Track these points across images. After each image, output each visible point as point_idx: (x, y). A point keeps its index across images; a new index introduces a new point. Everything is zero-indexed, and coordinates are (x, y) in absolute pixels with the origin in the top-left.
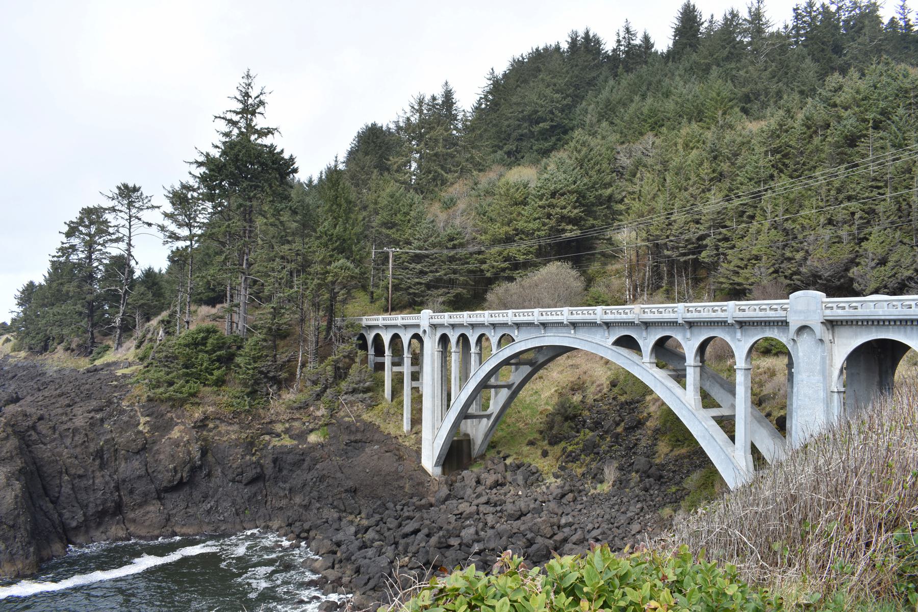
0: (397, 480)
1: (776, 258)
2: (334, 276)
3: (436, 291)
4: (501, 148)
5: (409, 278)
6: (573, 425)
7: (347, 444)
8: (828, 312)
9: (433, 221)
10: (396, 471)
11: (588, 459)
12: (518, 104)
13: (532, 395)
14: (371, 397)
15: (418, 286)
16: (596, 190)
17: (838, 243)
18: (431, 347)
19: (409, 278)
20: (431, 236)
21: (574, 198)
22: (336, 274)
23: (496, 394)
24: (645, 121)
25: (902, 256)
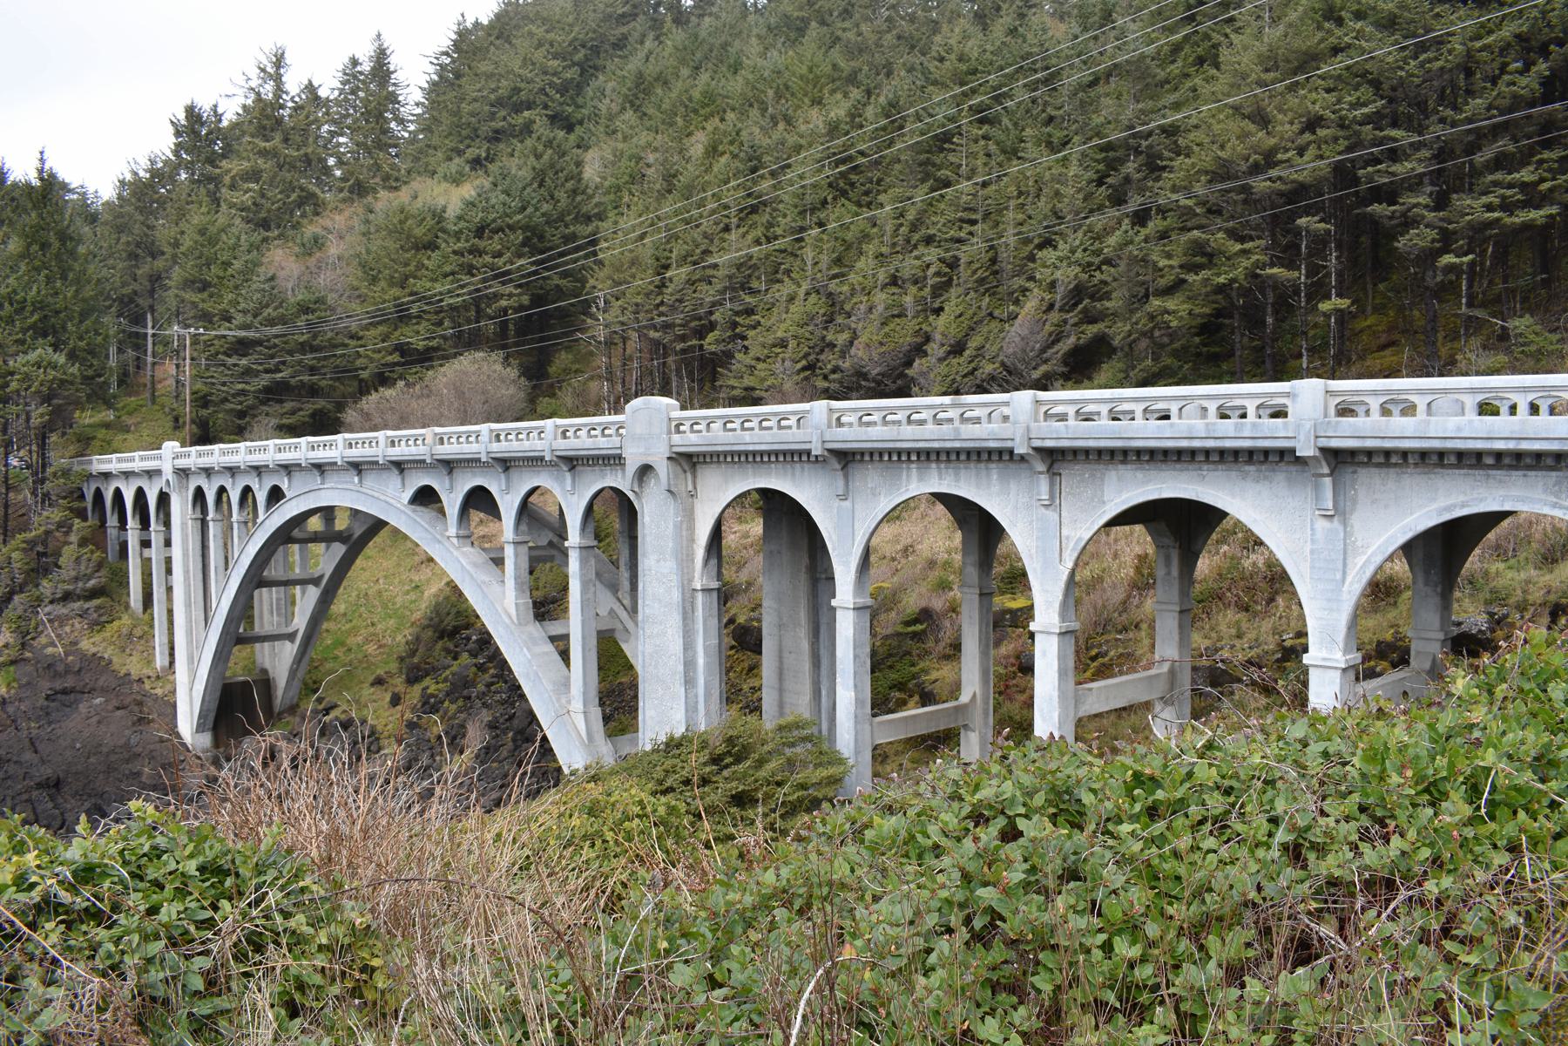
0: (128, 761)
1: (811, 343)
2: (23, 380)
3: (277, 407)
4: (460, 153)
5: (224, 384)
6: (451, 646)
7: (48, 698)
8: (676, 438)
9: (272, 278)
10: (127, 746)
11: (453, 707)
12: (489, 76)
13: (407, 593)
14: (98, 608)
15: (242, 399)
16: (566, 226)
17: (899, 316)
18: (180, 507)
19: (224, 384)
20: (267, 306)
21: (519, 237)
22: (27, 378)
23: (303, 593)
24: (695, 111)
25: (987, 339)
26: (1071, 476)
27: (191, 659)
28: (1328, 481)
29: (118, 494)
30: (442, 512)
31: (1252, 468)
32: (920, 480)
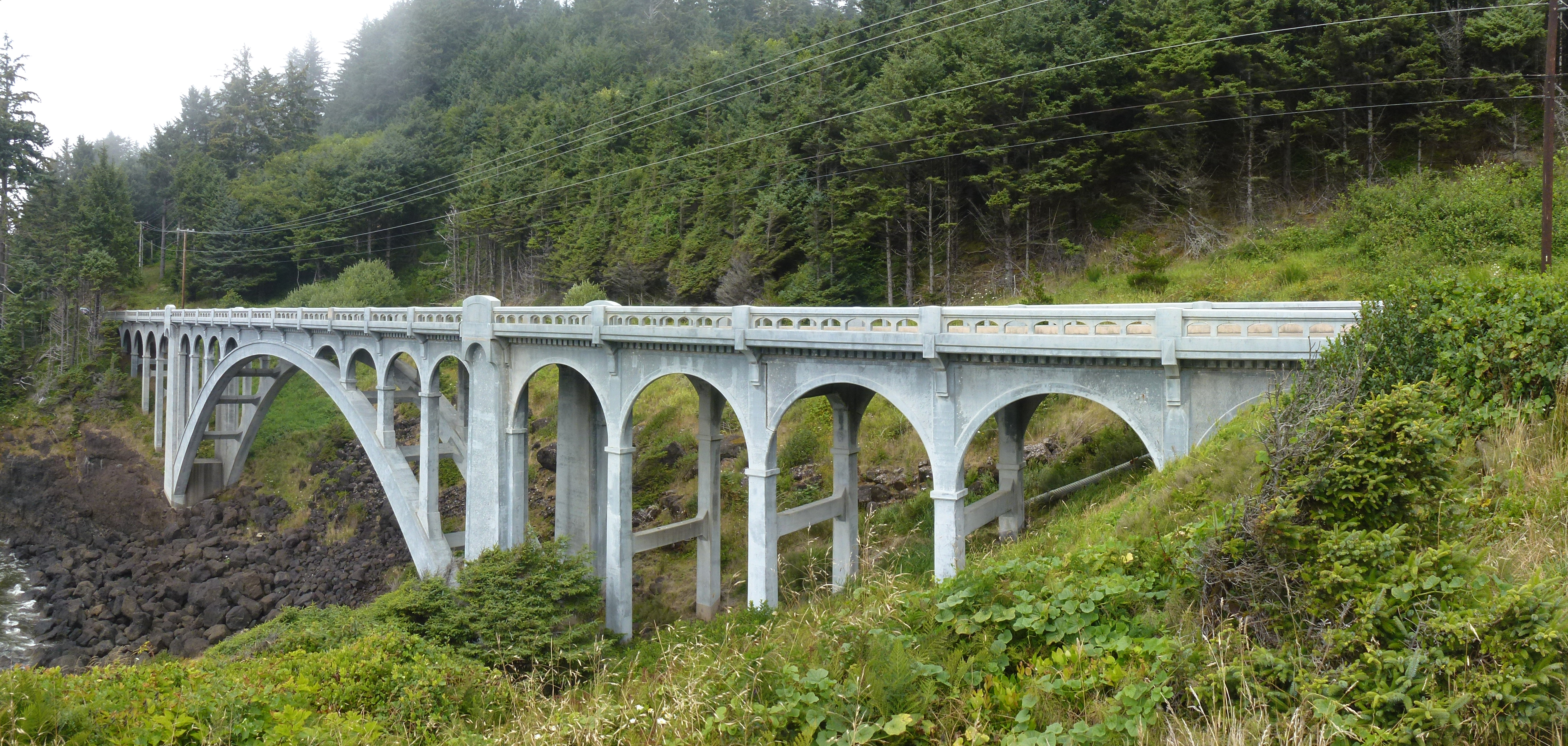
8: (498, 326)
18: (174, 346)
26: (775, 365)
27: (174, 445)
28: (944, 373)
29: (138, 335)
30: (336, 362)
31: (894, 364)
32: (669, 364)
